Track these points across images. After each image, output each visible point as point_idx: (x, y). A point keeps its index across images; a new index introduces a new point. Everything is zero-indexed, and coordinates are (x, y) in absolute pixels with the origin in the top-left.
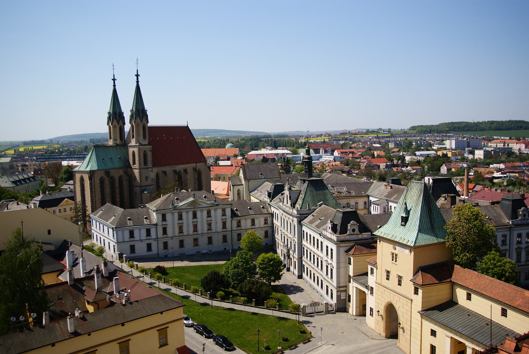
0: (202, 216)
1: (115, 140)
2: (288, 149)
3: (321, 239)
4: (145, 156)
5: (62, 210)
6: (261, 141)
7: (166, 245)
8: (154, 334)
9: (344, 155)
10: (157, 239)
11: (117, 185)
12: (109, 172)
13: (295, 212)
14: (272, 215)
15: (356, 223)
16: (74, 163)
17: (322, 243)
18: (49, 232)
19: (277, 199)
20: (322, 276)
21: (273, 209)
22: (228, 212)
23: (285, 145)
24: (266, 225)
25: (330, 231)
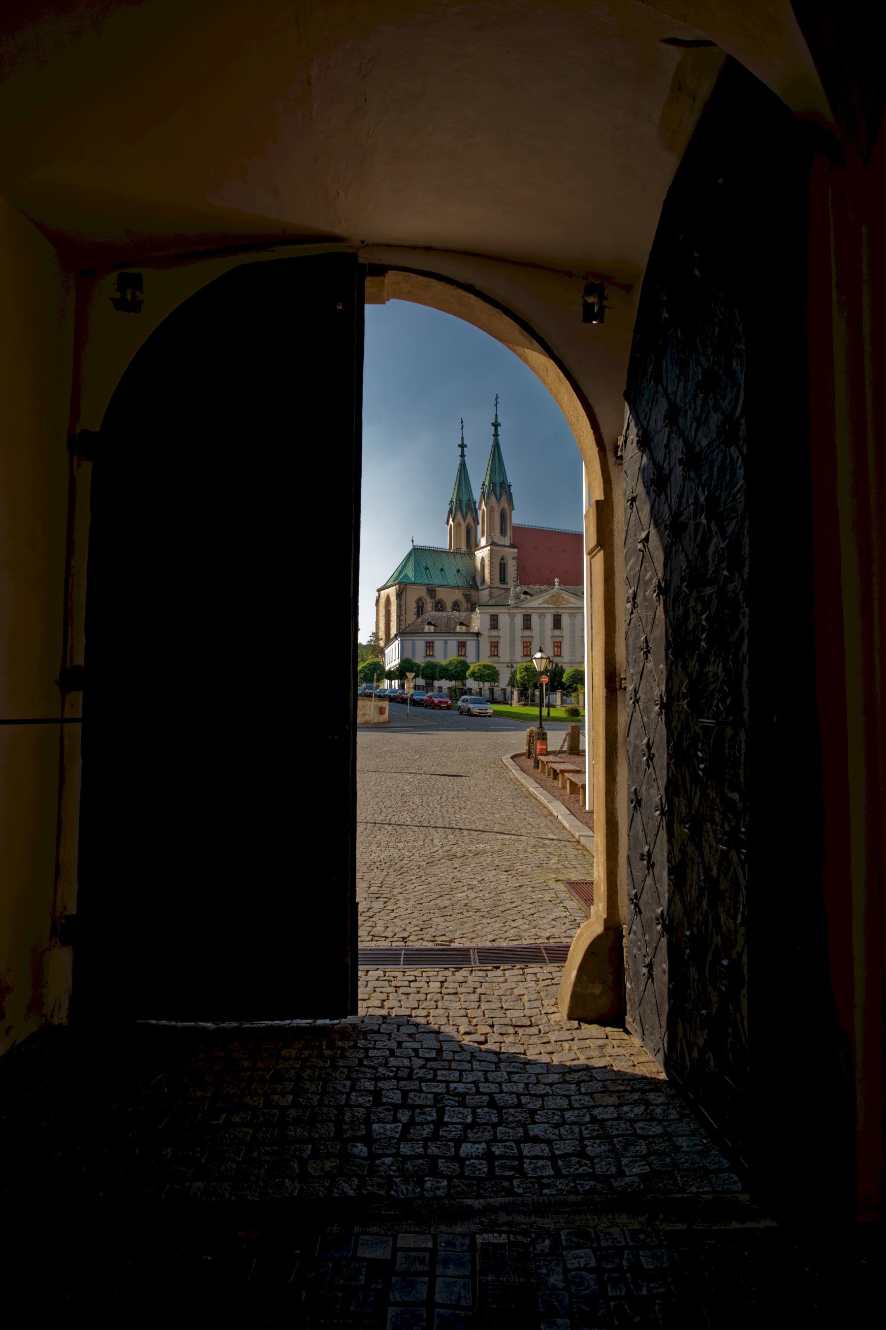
12: (434, 591)
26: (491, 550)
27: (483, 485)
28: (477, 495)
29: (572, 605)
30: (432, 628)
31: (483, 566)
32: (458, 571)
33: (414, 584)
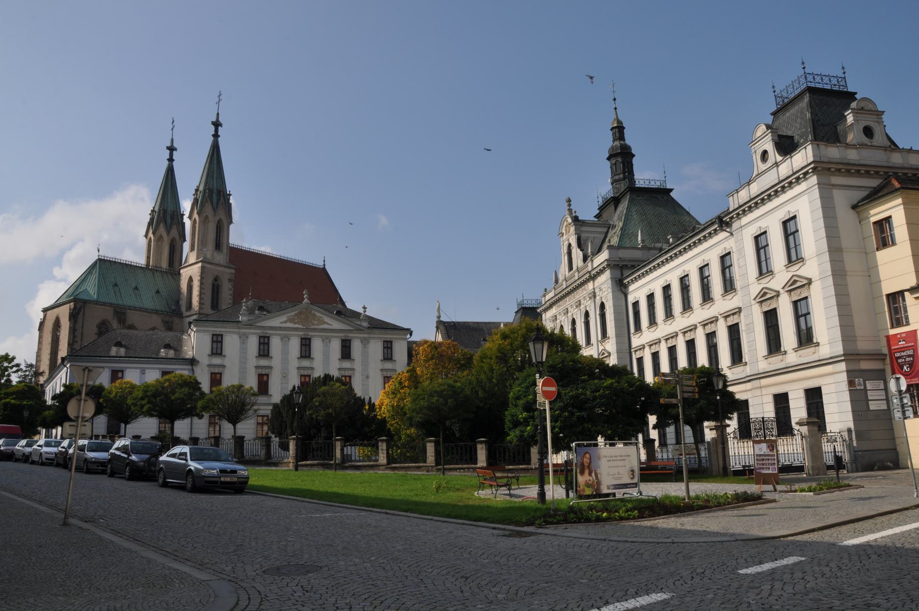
12: (124, 314)
26: (202, 267)
27: (197, 190)
28: (186, 205)
29: (325, 326)
30: (122, 351)
31: (190, 287)
32: (158, 292)
33: (96, 303)
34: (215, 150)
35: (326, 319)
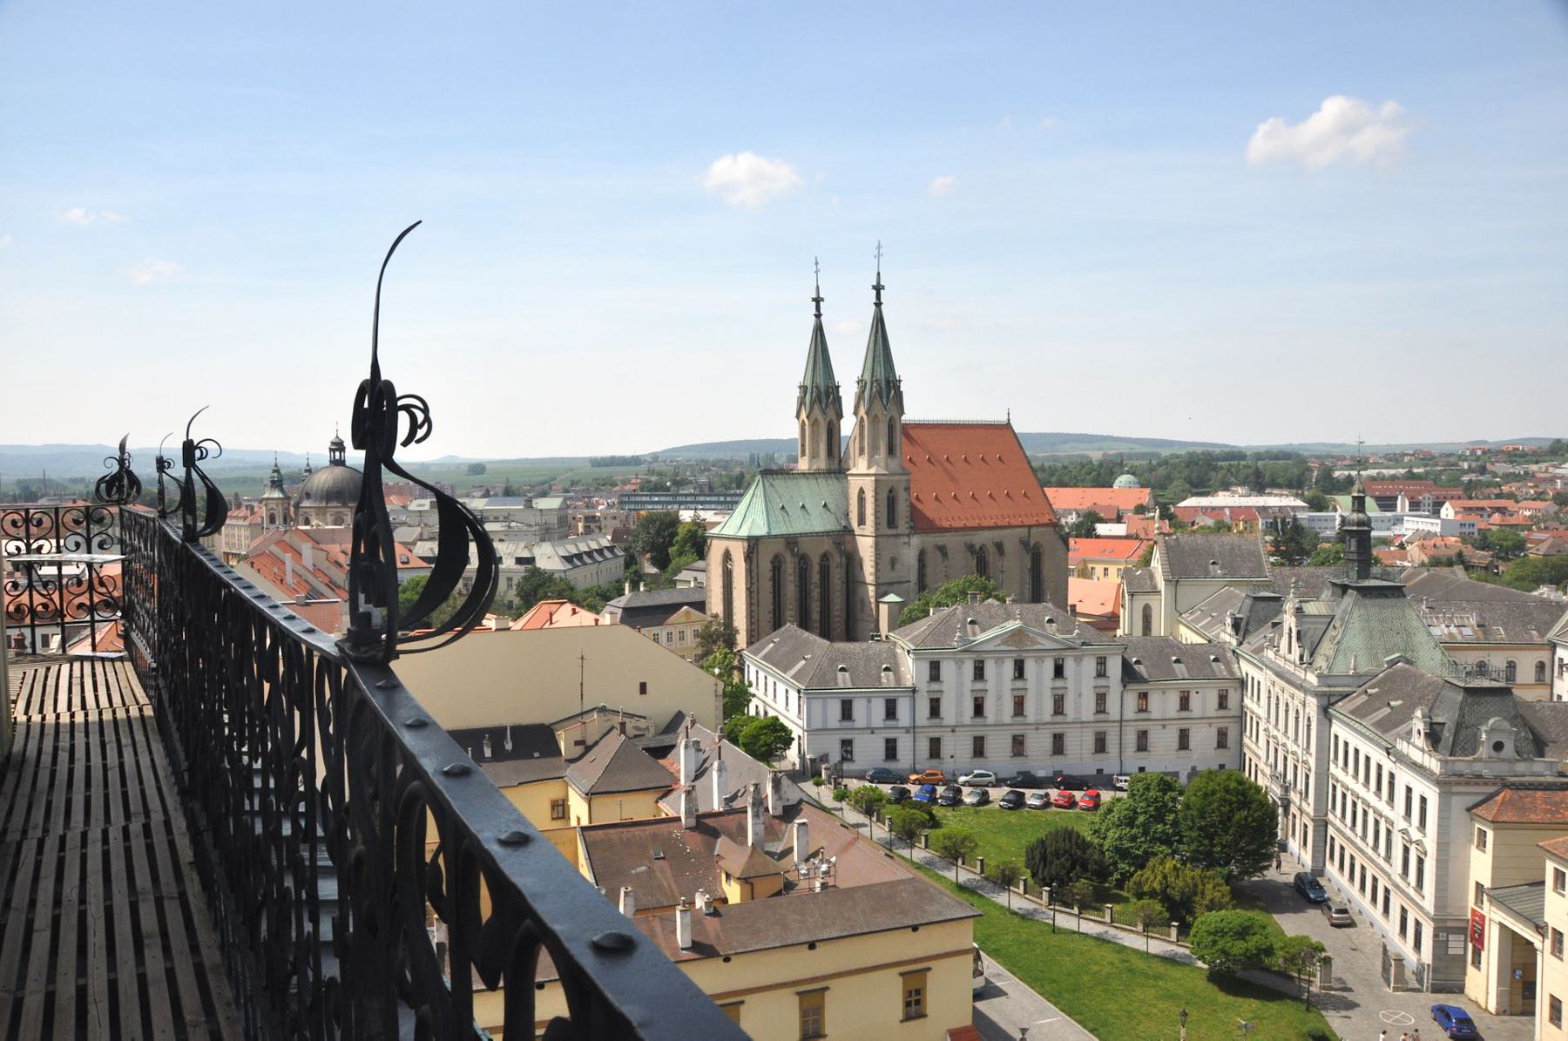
0: (1039, 673)
1: (814, 456)
2: (1297, 496)
3: (1388, 765)
4: (891, 503)
5: (676, 636)
6: (1215, 469)
7: (935, 744)
8: (891, 990)
9: (1473, 518)
10: (913, 729)
11: (815, 577)
12: (796, 543)
13: (1312, 679)
14: (1242, 683)
15: (1506, 725)
16: (708, 516)
17: (1392, 776)
18: (643, 688)
19: (1255, 639)
20: (1389, 876)
21: (1246, 668)
22: (1114, 668)
23: (1295, 484)
24: (1222, 713)
25: (1420, 741)
33: (769, 536)
34: (879, 322)
35: (1039, 639)
